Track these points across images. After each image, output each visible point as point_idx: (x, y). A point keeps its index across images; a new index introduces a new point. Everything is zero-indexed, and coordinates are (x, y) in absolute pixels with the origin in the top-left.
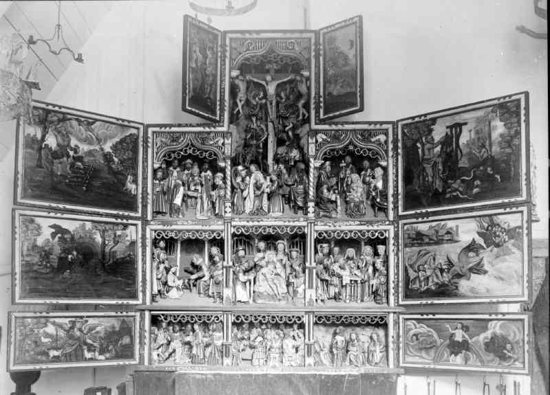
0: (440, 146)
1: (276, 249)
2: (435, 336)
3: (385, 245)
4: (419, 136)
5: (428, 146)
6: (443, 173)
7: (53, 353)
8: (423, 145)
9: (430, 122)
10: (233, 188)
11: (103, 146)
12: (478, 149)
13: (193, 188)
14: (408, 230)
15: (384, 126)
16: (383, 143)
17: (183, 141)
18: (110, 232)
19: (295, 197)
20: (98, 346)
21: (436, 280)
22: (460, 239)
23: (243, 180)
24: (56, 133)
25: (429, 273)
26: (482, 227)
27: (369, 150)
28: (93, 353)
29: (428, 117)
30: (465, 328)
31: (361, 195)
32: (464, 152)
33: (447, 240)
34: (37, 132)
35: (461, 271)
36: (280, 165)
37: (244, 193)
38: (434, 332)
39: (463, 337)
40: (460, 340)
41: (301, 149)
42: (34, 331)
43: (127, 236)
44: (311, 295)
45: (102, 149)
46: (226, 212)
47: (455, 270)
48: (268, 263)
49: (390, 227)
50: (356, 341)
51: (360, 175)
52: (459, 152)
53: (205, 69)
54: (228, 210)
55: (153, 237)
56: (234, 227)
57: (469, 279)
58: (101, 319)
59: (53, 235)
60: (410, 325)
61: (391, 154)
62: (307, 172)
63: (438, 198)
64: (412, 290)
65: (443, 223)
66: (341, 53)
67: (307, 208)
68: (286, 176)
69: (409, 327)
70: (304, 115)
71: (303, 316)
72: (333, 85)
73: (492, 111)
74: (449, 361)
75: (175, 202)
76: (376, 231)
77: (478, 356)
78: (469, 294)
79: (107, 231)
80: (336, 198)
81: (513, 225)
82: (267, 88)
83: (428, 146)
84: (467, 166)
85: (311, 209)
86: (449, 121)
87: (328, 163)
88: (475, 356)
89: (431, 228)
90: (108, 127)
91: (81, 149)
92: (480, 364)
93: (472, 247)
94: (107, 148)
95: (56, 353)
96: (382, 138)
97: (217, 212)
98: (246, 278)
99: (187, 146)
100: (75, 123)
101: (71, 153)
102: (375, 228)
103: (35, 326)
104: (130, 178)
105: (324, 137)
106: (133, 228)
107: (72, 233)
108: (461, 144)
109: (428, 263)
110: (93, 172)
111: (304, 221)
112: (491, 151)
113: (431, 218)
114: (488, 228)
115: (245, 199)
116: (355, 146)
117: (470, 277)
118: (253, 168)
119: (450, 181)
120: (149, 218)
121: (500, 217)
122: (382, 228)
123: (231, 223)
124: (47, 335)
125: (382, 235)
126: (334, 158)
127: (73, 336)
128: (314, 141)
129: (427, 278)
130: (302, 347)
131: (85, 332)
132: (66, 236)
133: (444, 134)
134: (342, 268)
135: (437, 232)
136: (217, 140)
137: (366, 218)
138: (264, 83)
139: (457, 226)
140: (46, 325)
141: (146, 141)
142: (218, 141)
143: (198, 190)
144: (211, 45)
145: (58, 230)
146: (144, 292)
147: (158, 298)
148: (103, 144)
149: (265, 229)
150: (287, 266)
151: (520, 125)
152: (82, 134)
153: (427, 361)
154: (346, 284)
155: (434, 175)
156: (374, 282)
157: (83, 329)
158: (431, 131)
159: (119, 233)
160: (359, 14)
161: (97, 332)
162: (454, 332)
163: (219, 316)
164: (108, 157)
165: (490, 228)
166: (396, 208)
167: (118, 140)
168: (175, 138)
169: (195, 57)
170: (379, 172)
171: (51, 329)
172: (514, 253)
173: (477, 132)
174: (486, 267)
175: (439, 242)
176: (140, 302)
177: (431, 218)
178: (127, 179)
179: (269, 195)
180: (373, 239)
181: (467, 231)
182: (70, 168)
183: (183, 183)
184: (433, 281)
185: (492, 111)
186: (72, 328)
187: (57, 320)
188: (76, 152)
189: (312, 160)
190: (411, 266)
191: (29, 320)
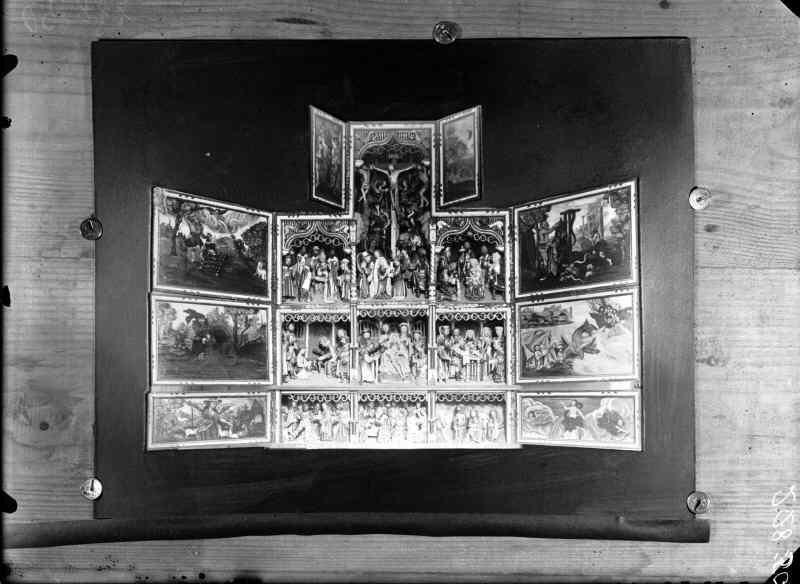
5: (543, 231)
7: (189, 432)
8: (538, 231)
10: (358, 272)
13: (320, 273)
21: (551, 360)
23: (368, 265)
25: (544, 352)
27: (487, 235)
30: (579, 405)
39: (577, 413)
45: (233, 237)
48: (392, 344)
51: (479, 261)
54: (354, 294)
57: (582, 358)
59: (188, 319)
61: (508, 239)
63: (553, 282)
65: (557, 305)
67: (428, 292)
70: (425, 203)
72: (452, 175)
78: (583, 373)
83: (543, 231)
85: (432, 293)
89: (546, 309)
93: (585, 328)
94: (238, 236)
95: (192, 432)
96: (499, 224)
100: (207, 212)
101: (204, 241)
110: (226, 259)
113: (545, 301)
119: (564, 265)
120: (279, 302)
124: (183, 415)
125: (500, 316)
126: (454, 244)
129: (543, 358)
130: (425, 424)
132: (200, 320)
134: (462, 348)
138: (386, 172)
140: (182, 406)
141: (275, 229)
145: (192, 314)
146: (274, 373)
147: (288, 379)
156: (493, 362)
158: (545, 217)
159: (250, 317)
161: (231, 412)
166: (513, 291)
169: (320, 147)
171: (187, 409)
173: (590, 218)
175: (553, 323)
177: (545, 301)
185: (604, 198)
186: (207, 408)
187: (193, 400)
189: (433, 246)
190: (528, 346)
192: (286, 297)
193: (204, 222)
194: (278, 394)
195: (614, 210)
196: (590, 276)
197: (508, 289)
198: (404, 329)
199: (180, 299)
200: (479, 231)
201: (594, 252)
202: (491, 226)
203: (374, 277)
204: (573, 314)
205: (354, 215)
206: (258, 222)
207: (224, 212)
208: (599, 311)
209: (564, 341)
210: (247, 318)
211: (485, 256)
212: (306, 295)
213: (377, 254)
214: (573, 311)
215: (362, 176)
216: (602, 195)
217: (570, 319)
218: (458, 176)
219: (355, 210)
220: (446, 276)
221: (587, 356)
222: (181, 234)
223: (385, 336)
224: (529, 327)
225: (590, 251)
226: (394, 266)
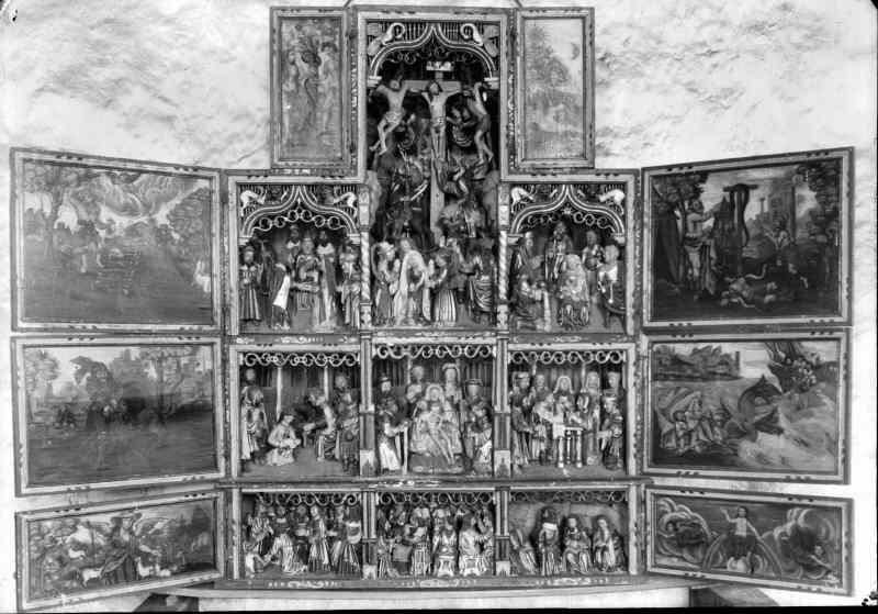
1: (443, 379)
2: (705, 526)
3: (621, 372)
4: (677, 197)
5: (692, 216)
6: (716, 265)
7: (89, 574)
8: (685, 214)
9: (698, 177)
10: (373, 278)
11: (154, 217)
12: (774, 231)
13: (303, 275)
14: (658, 352)
15: (621, 178)
16: (619, 204)
17: (286, 198)
19: (475, 296)
20: (160, 555)
21: (702, 437)
22: (742, 374)
23: (391, 266)
24: (76, 202)
25: (692, 425)
26: (776, 358)
27: (597, 216)
28: (151, 568)
29: (694, 169)
31: (584, 290)
32: (752, 233)
33: (721, 374)
34: (39, 202)
35: (743, 427)
36: (450, 240)
37: (391, 287)
39: (749, 530)
40: (744, 534)
41: (485, 211)
42: (56, 542)
43: (198, 364)
44: (503, 460)
45: (152, 221)
46: (362, 321)
47: (733, 424)
48: (430, 403)
49: (628, 345)
50: (576, 530)
51: (581, 256)
52: (743, 233)
54: (367, 318)
55: (241, 363)
56: (377, 346)
57: (754, 440)
58: (162, 509)
60: (663, 506)
61: (631, 224)
62: (495, 251)
63: (710, 303)
64: (665, 452)
65: (715, 346)
66: (555, 60)
67: (496, 314)
68: (461, 259)
69: (662, 508)
71: (492, 494)
72: (539, 112)
73: (798, 172)
74: (725, 567)
75: (275, 303)
76: (607, 352)
77: (772, 563)
78: (754, 463)
79: (166, 359)
80: (543, 295)
81: (824, 359)
84: (754, 257)
85: (502, 317)
86: (729, 180)
87: (528, 235)
88: (766, 562)
89: (696, 351)
90: (161, 182)
91: (117, 225)
92: (773, 575)
93: (759, 389)
94: (162, 217)
96: (618, 195)
97: (347, 321)
98: (396, 430)
99: (294, 207)
100: (106, 181)
101: (102, 233)
102: (606, 346)
103: (59, 533)
104: (200, 266)
106: (206, 350)
107: (108, 368)
108: (746, 219)
109: (690, 409)
110: (134, 265)
111: (491, 336)
112: (794, 236)
113: (695, 337)
114: (786, 359)
115: (393, 296)
116: (575, 210)
117: (756, 438)
119: (727, 279)
121: (804, 344)
122: (616, 346)
123: (370, 340)
124: (78, 546)
125: (616, 357)
126: (541, 228)
127: (120, 544)
128: (507, 201)
129: (688, 434)
130: (491, 543)
131: (137, 533)
133: (720, 200)
134: (552, 409)
135: (705, 359)
137: (590, 329)
139: (738, 353)
140: (74, 529)
141: (224, 200)
143: (312, 279)
144: (327, 39)
145: (86, 365)
146: (227, 456)
147: (251, 466)
148: (154, 213)
149: (426, 349)
150: (461, 408)
151: (839, 200)
152: (119, 199)
153: (690, 565)
154: (559, 437)
155: (702, 265)
156: (605, 435)
158: (698, 192)
160: (591, 5)
161: (158, 532)
162: (733, 521)
163: (354, 495)
164: (164, 233)
165: (789, 361)
166: (638, 314)
167: (178, 202)
168: (273, 192)
169: (293, 71)
170: (611, 252)
171: (83, 535)
172: (825, 404)
173: (773, 204)
174: (783, 423)
175: (710, 376)
176: (222, 474)
177: (695, 337)
178: (195, 266)
179: (431, 290)
181: (754, 363)
182: (101, 260)
183: (288, 268)
184: (698, 440)
185: (798, 172)
186: (116, 529)
187: (92, 519)
188: (110, 231)
189: (503, 233)
191: (49, 524)
192: (245, 321)
193: (101, 200)
194: (235, 492)
195: (814, 194)
196: (770, 303)
197: (630, 311)
199: (65, 341)
200: (584, 206)
201: (779, 263)
202: (603, 198)
203: (402, 287)
204: (742, 365)
205: (366, 177)
207: (135, 178)
208: (784, 363)
209: (725, 410)
211: (592, 248)
212: (280, 316)
214: (742, 360)
216: (796, 167)
217: (734, 372)
219: (369, 166)
220: (525, 285)
221: (761, 435)
222: (61, 226)
223: (418, 388)
224: (666, 378)
225: (772, 260)
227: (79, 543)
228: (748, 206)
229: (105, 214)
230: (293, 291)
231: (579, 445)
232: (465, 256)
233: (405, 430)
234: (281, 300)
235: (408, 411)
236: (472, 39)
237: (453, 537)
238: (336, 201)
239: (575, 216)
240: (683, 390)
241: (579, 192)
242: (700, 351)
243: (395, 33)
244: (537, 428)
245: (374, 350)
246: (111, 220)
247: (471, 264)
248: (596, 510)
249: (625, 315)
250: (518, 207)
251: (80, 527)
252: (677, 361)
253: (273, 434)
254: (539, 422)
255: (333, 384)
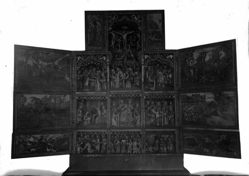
0: (196, 61)
2: (197, 140)
5: (192, 61)
18: (58, 98)
21: (195, 117)
24: (32, 59)
25: (193, 114)
26: (216, 96)
38: (195, 138)
39: (209, 140)
40: (208, 142)
43: (66, 99)
45: (54, 64)
53: (96, 30)
57: (210, 118)
59: (32, 101)
60: (185, 135)
70: (139, 47)
74: (203, 151)
79: (57, 98)
82: (123, 36)
93: (211, 104)
95: (34, 150)
99: (91, 60)
101: (40, 67)
105: (148, 56)
108: (206, 60)
116: (160, 60)
118: (118, 69)
124: (31, 142)
131: (47, 140)
132: (38, 101)
136: (103, 58)
138: (121, 34)
139: (205, 95)
140: (30, 138)
142: (103, 58)
144: (98, 19)
157: (47, 139)
158: (192, 55)
159: (62, 98)
162: (205, 138)
171: (32, 139)
173: (213, 56)
174: (219, 113)
180: (168, 99)
182: (39, 73)
184: (194, 117)
186: (41, 139)
188: (42, 66)
198: (130, 102)
202: (168, 57)
206: (66, 56)
210: (60, 99)
213: (118, 69)
215: (112, 35)
218: (154, 37)
226: (126, 75)
227: (30, 141)
228: (206, 57)
229: (40, 62)
230: (90, 82)
231: (163, 120)
232: (133, 72)
233: (119, 116)
234: (87, 84)
235: (120, 111)
236: (134, 19)
237: (131, 143)
238: (101, 59)
239: (160, 61)
240: (190, 105)
241: (162, 56)
242: (194, 95)
243: (116, 18)
244: (152, 115)
245: (110, 96)
246: (42, 63)
247: (135, 74)
248: (167, 136)
249: (174, 86)
250: (146, 60)
251: (31, 137)
252: (188, 98)
253: (84, 118)
254: (152, 114)
255: (100, 104)
